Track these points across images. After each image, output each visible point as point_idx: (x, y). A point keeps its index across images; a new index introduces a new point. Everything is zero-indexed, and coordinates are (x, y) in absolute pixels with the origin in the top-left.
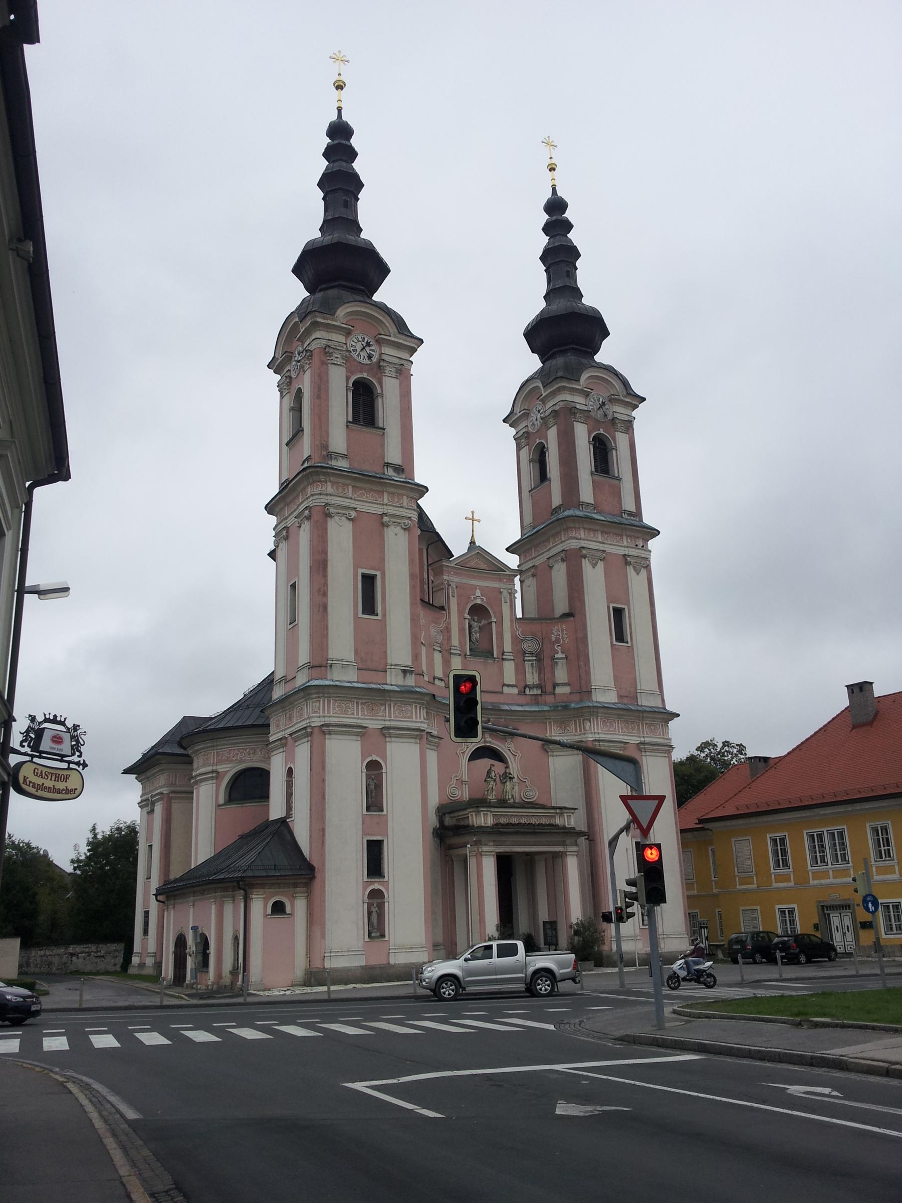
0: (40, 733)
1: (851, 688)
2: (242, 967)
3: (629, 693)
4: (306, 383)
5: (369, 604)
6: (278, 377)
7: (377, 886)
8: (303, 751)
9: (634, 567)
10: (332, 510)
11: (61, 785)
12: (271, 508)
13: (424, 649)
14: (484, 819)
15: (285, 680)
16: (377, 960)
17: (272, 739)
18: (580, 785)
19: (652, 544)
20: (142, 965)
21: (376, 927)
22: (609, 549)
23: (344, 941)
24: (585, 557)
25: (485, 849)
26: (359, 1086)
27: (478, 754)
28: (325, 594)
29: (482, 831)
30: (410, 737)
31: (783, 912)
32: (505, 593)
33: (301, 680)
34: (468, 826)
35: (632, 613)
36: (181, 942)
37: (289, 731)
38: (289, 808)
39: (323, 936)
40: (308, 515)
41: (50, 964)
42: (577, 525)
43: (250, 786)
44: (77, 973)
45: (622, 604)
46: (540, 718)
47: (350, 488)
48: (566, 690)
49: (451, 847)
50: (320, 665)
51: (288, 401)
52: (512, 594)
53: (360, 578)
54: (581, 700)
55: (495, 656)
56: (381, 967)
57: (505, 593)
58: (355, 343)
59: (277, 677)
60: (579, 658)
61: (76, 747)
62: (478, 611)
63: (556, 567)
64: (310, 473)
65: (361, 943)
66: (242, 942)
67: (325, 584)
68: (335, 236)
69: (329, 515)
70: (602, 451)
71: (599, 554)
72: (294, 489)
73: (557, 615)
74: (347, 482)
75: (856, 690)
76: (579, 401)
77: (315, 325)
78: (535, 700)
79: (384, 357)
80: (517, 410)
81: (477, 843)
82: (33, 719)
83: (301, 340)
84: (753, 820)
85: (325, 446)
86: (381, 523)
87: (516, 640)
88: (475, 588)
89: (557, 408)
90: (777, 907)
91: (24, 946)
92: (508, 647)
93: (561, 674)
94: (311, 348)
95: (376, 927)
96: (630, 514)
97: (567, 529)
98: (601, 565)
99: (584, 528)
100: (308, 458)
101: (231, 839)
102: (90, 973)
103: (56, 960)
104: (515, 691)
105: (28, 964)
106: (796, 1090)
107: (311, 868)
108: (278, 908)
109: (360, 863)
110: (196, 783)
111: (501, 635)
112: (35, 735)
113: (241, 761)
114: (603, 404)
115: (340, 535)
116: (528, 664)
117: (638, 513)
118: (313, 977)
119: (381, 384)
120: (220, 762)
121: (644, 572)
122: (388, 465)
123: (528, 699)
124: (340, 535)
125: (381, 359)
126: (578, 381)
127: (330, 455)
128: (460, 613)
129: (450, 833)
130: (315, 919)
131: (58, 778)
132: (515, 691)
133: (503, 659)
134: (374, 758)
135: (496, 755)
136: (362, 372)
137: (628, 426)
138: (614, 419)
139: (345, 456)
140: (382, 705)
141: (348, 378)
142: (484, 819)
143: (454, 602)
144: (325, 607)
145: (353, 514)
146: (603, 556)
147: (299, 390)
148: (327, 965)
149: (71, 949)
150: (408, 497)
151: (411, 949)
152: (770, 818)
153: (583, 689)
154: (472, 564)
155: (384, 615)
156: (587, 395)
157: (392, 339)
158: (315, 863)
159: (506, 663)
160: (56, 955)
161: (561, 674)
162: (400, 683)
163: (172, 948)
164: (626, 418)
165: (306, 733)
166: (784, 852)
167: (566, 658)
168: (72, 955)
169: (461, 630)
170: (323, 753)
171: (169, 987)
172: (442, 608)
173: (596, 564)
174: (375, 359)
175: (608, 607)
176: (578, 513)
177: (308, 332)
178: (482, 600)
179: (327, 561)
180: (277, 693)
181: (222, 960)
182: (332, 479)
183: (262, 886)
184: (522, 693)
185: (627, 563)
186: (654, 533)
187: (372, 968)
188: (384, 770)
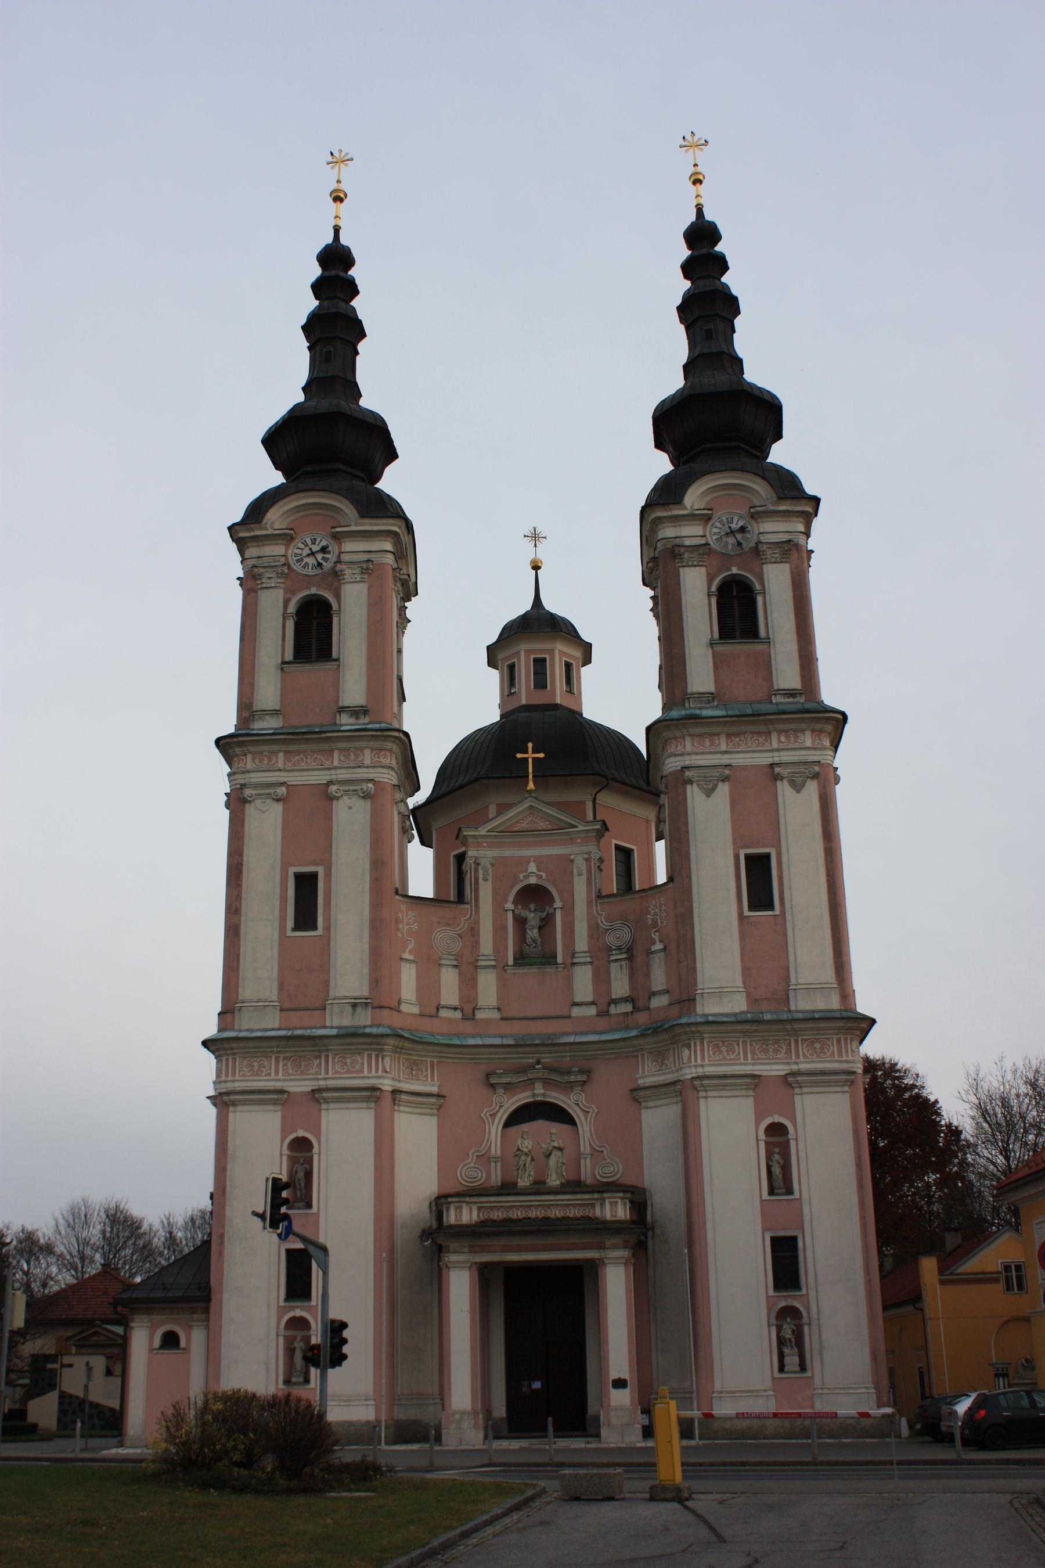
7: (298, 1313)
9: (698, 785)
18: (681, 1150)
24: (691, 782)
27: (520, 1116)
30: (836, 1083)
35: (784, 858)
42: (678, 733)
45: (764, 846)
47: (281, 755)
55: (560, 960)
60: (683, 949)
62: (534, 895)
64: (396, 737)
68: (324, 404)
71: (716, 773)
74: (276, 747)
79: (763, 538)
86: (326, 796)
87: (595, 931)
88: (526, 860)
92: (582, 943)
93: (659, 978)
98: (723, 790)
99: (692, 735)
104: (592, 1011)
108: (170, 1341)
109: (274, 1281)
116: (614, 967)
119: (338, 597)
122: (342, 710)
125: (339, 561)
128: (498, 903)
132: (592, 1011)
133: (573, 964)
134: (301, 1133)
135: (560, 1115)
136: (308, 588)
140: (316, 1057)
150: (372, 750)
153: (686, 1000)
154: (524, 825)
155: (327, 929)
157: (353, 528)
159: (578, 969)
167: (664, 949)
169: (499, 929)
173: (803, 785)
175: (737, 857)
178: (540, 877)
179: (241, 864)
182: (252, 749)
183: (148, 1311)
184: (603, 1013)
185: (777, 778)
188: (315, 1150)
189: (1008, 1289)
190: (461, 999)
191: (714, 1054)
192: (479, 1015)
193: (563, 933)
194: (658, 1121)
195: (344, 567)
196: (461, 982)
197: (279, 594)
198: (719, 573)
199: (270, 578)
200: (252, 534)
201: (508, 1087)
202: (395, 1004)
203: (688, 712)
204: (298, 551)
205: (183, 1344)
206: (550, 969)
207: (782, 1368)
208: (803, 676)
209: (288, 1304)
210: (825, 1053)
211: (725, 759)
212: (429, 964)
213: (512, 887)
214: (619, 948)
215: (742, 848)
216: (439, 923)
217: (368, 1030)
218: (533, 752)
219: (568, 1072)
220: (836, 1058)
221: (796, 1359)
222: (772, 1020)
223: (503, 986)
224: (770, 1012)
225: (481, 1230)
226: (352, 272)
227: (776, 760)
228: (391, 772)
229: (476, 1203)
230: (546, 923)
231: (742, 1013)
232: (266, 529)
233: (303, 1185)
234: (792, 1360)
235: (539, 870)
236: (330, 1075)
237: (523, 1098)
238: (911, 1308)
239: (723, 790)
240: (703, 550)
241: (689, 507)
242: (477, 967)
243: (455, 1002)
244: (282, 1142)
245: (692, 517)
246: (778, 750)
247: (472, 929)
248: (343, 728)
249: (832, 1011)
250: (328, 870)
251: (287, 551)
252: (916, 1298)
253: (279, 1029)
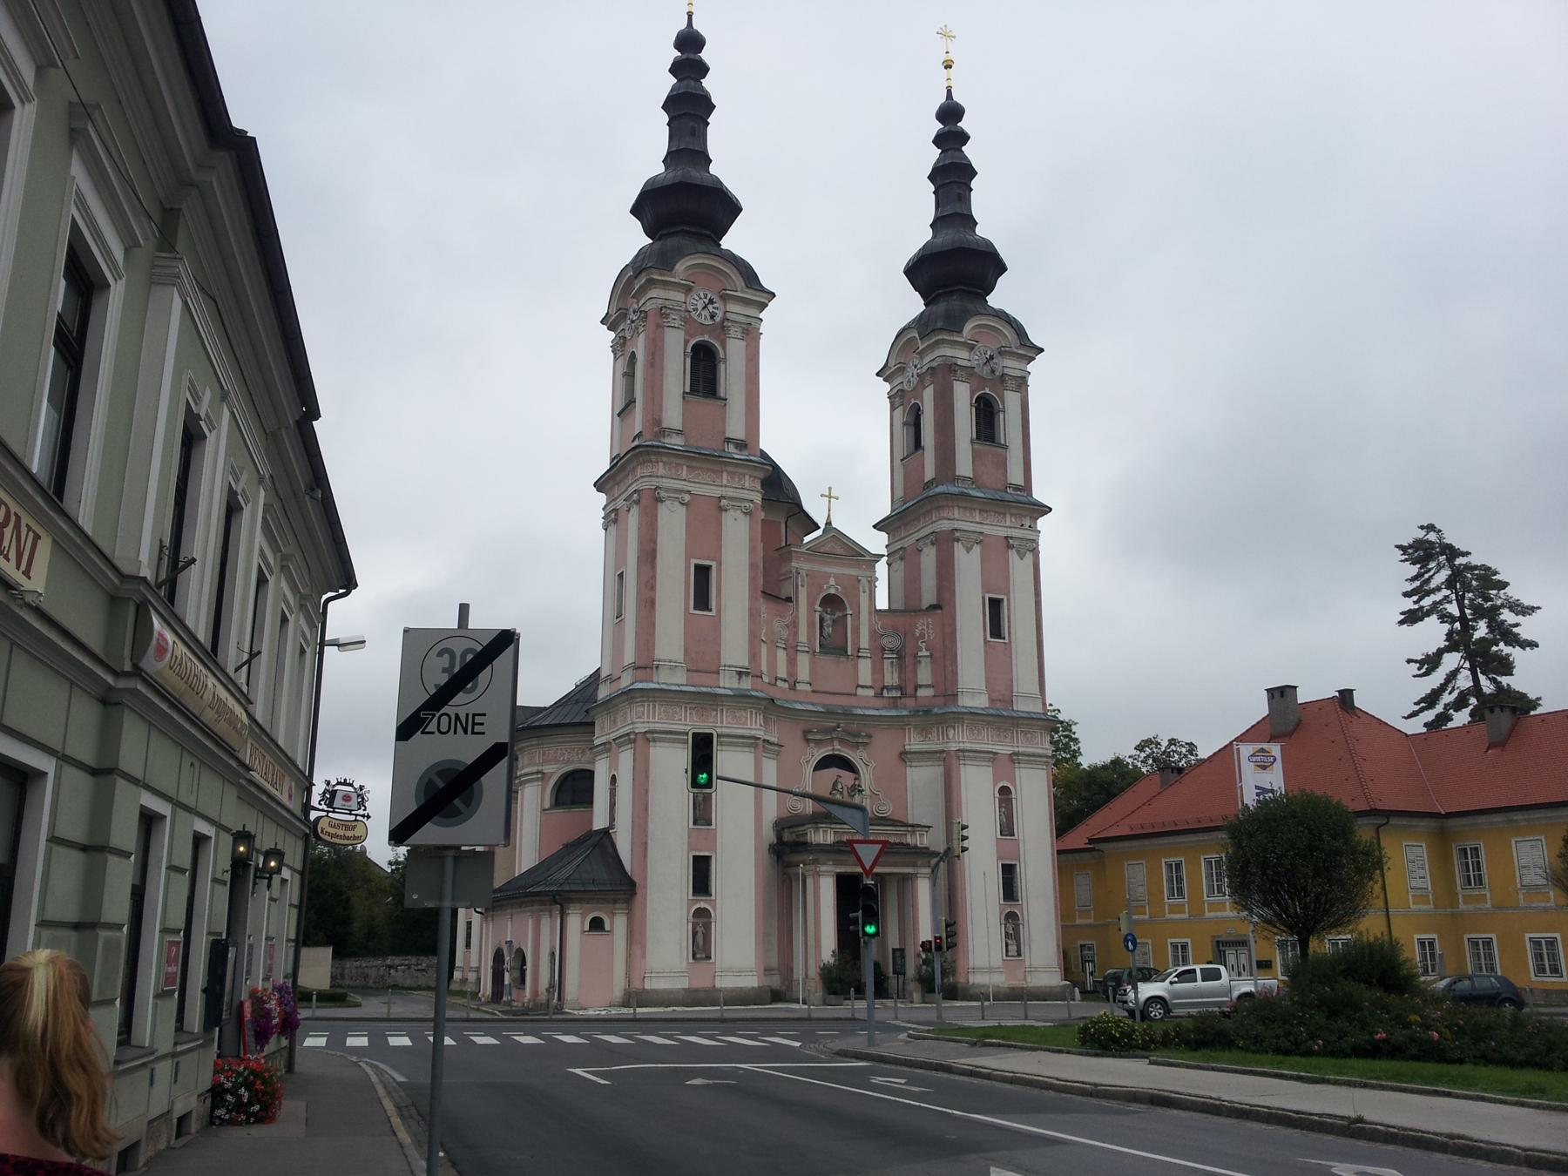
0: (334, 793)
1: (1271, 692)
2: (558, 985)
3: (1002, 693)
4: (640, 347)
5: (702, 598)
6: (612, 335)
7: (702, 905)
8: (626, 758)
10: (663, 494)
11: (350, 834)
12: (600, 485)
13: (764, 648)
14: (823, 836)
15: (611, 679)
16: (702, 983)
17: (597, 742)
19: (1042, 523)
20: (464, 981)
21: (701, 947)
22: (986, 529)
23: (666, 962)
25: (823, 868)
26: (578, 1071)
27: (824, 763)
28: (653, 588)
29: (822, 849)
30: (744, 745)
31: (1175, 947)
32: (864, 581)
33: (626, 681)
34: (805, 843)
36: (498, 957)
37: (613, 736)
38: (612, 819)
39: (644, 956)
40: (637, 499)
41: (366, 976)
43: (575, 790)
44: (395, 987)
46: (898, 724)
48: (930, 692)
49: (789, 865)
50: (646, 666)
51: (622, 364)
52: (872, 582)
54: (945, 705)
56: (706, 991)
57: (864, 581)
58: (696, 301)
59: (603, 674)
60: (946, 656)
61: (362, 804)
62: (831, 602)
63: (926, 550)
65: (685, 963)
66: (559, 959)
67: (654, 577)
69: (659, 500)
70: (987, 413)
71: (974, 537)
72: (623, 467)
73: (925, 605)
75: (1277, 695)
76: (962, 356)
77: (651, 283)
78: (894, 703)
79: (729, 316)
80: (892, 363)
81: (816, 862)
82: (328, 783)
83: (637, 296)
84: (1147, 842)
85: (658, 422)
86: (719, 507)
87: (874, 635)
88: (828, 576)
89: (934, 364)
90: (1416, 936)
91: (337, 955)
92: (864, 642)
93: (924, 674)
94: (648, 307)
95: (701, 947)
96: (1017, 488)
97: (938, 508)
98: (977, 549)
100: (639, 435)
101: (556, 847)
102: (411, 988)
103: (372, 972)
104: (871, 693)
105: (342, 976)
106: (878, 1080)
107: (633, 884)
108: (597, 925)
110: (521, 783)
112: (330, 796)
113: (568, 762)
114: (992, 357)
115: (672, 522)
116: (887, 662)
117: (1027, 487)
118: (634, 997)
119: (724, 348)
120: (545, 762)
121: (1029, 556)
122: (729, 440)
123: (885, 702)
124: (672, 522)
125: (725, 319)
126: (960, 332)
127: (663, 432)
128: (810, 604)
129: (787, 851)
130: (635, 937)
131: (347, 828)
132: (871, 693)
137: (1021, 383)
138: (1003, 375)
139: (679, 433)
141: (686, 342)
142: (823, 836)
143: (803, 593)
144: (652, 603)
145: (687, 498)
146: (981, 539)
147: (633, 355)
148: (647, 986)
149: (388, 962)
151: (739, 972)
152: (1165, 840)
153: (949, 692)
154: (827, 549)
155: (719, 611)
156: (971, 348)
158: (635, 879)
159: (861, 661)
160: (372, 966)
161: (924, 674)
162: (735, 686)
163: (490, 963)
164: (1019, 374)
165: (629, 739)
166: (1179, 880)
168: (390, 967)
169: (811, 625)
170: (647, 761)
171: (487, 1003)
172: (789, 600)
174: (718, 319)
176: (952, 489)
177: (643, 290)
180: (603, 693)
181: (540, 976)
182: (730, 469)
183: (580, 901)
184: (879, 695)
185: (1009, 546)
186: (1045, 510)
187: (696, 990)
192: (799, 687)
194: (921, 779)
201: (818, 742)
205: (607, 927)
206: (843, 659)
211: (978, 528)
214: (891, 650)
219: (858, 735)
222: (1002, 717)
226: (706, 83)
230: (840, 623)
239: (977, 549)
245: (964, 345)
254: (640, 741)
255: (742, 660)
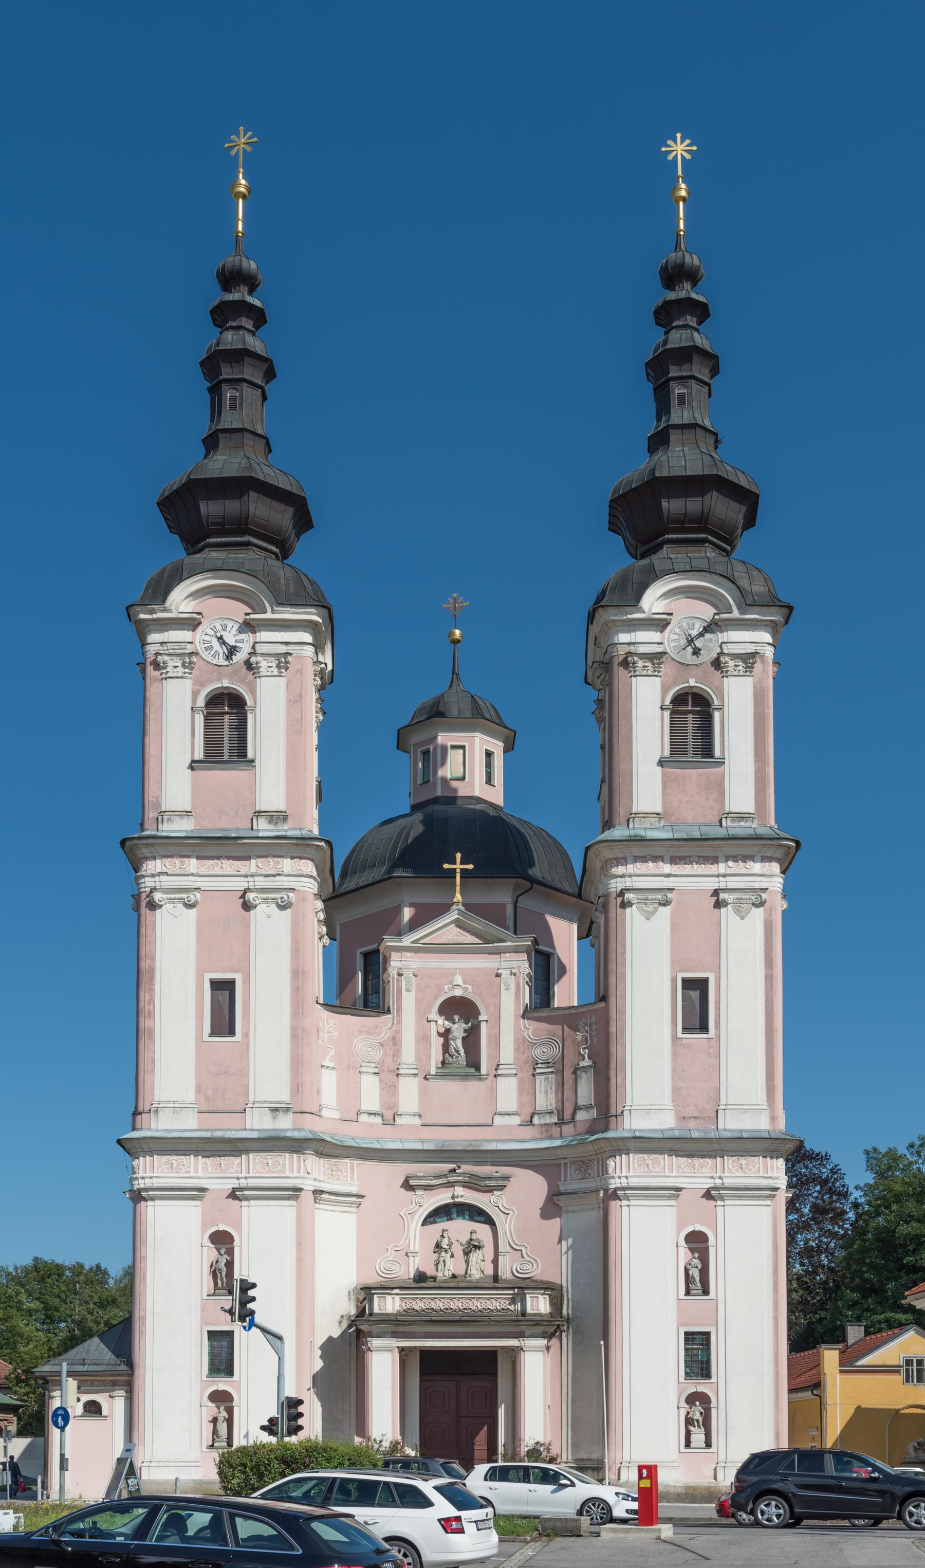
5: (224, 1021)
7: (221, 1387)
45: (703, 971)
53: (207, 986)
55: (484, 1070)
62: (459, 1008)
79: (726, 649)
87: (522, 1044)
92: (507, 1054)
104: (516, 1120)
111: (496, 1041)
119: (253, 692)
122: (258, 814)
125: (253, 653)
132: (516, 1120)
134: (698, 1228)
136: (219, 680)
141: (195, 695)
155: (246, 1035)
157: (269, 615)
161: (585, 1091)
169: (422, 1039)
178: (466, 989)
187: (694, 1488)
189: (907, 1381)
190: (382, 1104)
191: (639, 1166)
192: (399, 1121)
193: (489, 1046)
195: (259, 658)
196: (382, 1089)
197: (187, 685)
198: (675, 684)
199: (175, 667)
200: (155, 616)
202: (315, 1109)
203: (632, 833)
204: (207, 638)
205: (105, 1412)
207: (688, 1444)
208: (757, 800)
209: (210, 1379)
210: (750, 1170)
212: (350, 1069)
213: (436, 999)
214: (547, 1064)
215: (680, 971)
216: (360, 1031)
217: (289, 1134)
218: (461, 863)
220: (761, 1174)
221: (703, 1437)
223: (424, 1095)
224: (698, 1130)
225: (403, 1318)
227: (723, 885)
228: (312, 881)
229: (398, 1294)
231: (670, 1129)
232: (170, 611)
233: (224, 1274)
234: (698, 1437)
235: (464, 983)
236: (251, 1174)
237: (442, 1197)
238: (809, 1394)
240: (656, 658)
241: (646, 610)
242: (398, 1075)
243: (376, 1108)
244: (203, 1234)
246: (724, 876)
247: (394, 1038)
248: (260, 835)
249: (760, 1131)
250: (247, 977)
251: (194, 637)
252: (817, 1386)
253: (200, 1130)
254: (307, 1198)
255: (284, 1095)
